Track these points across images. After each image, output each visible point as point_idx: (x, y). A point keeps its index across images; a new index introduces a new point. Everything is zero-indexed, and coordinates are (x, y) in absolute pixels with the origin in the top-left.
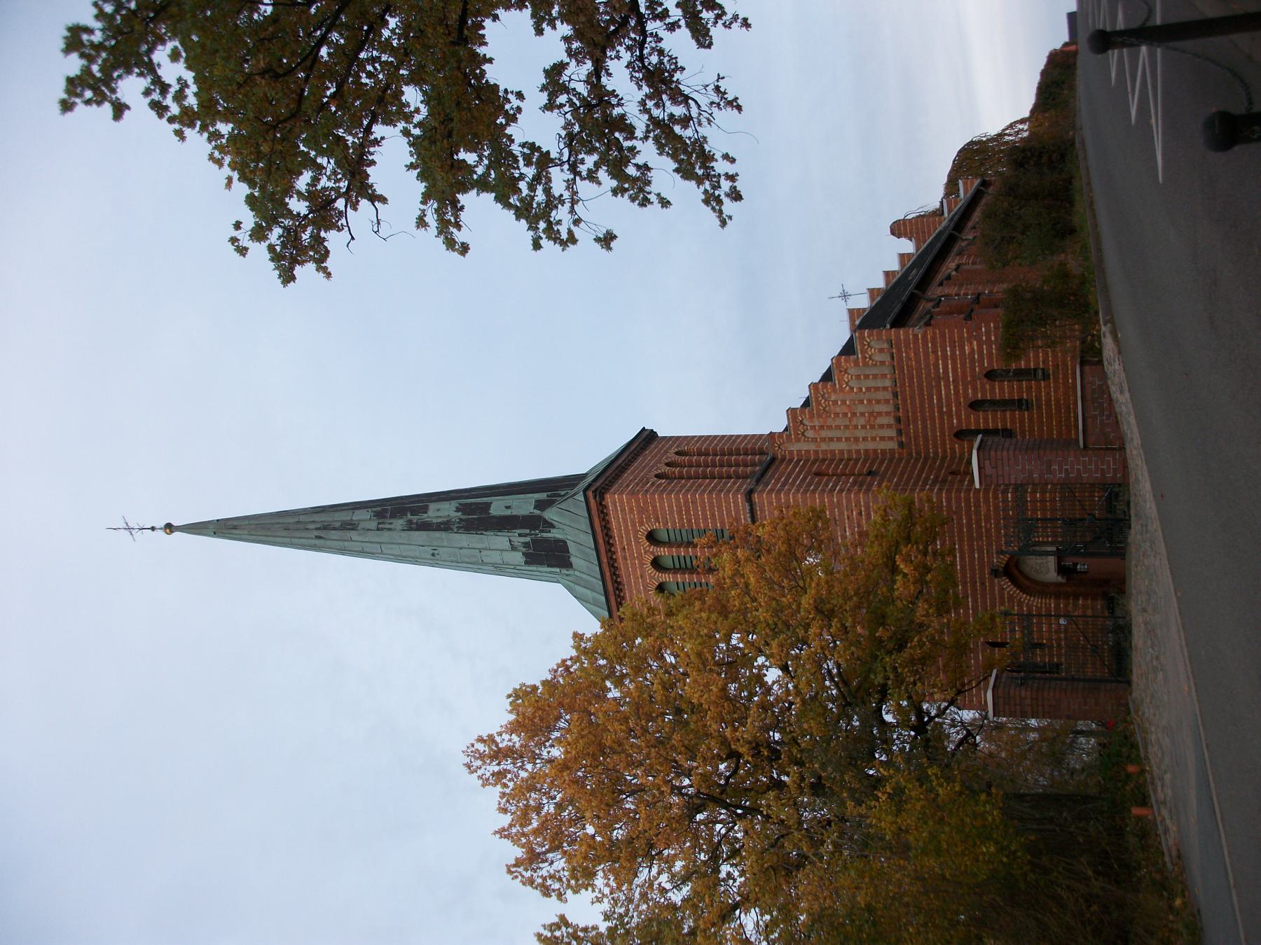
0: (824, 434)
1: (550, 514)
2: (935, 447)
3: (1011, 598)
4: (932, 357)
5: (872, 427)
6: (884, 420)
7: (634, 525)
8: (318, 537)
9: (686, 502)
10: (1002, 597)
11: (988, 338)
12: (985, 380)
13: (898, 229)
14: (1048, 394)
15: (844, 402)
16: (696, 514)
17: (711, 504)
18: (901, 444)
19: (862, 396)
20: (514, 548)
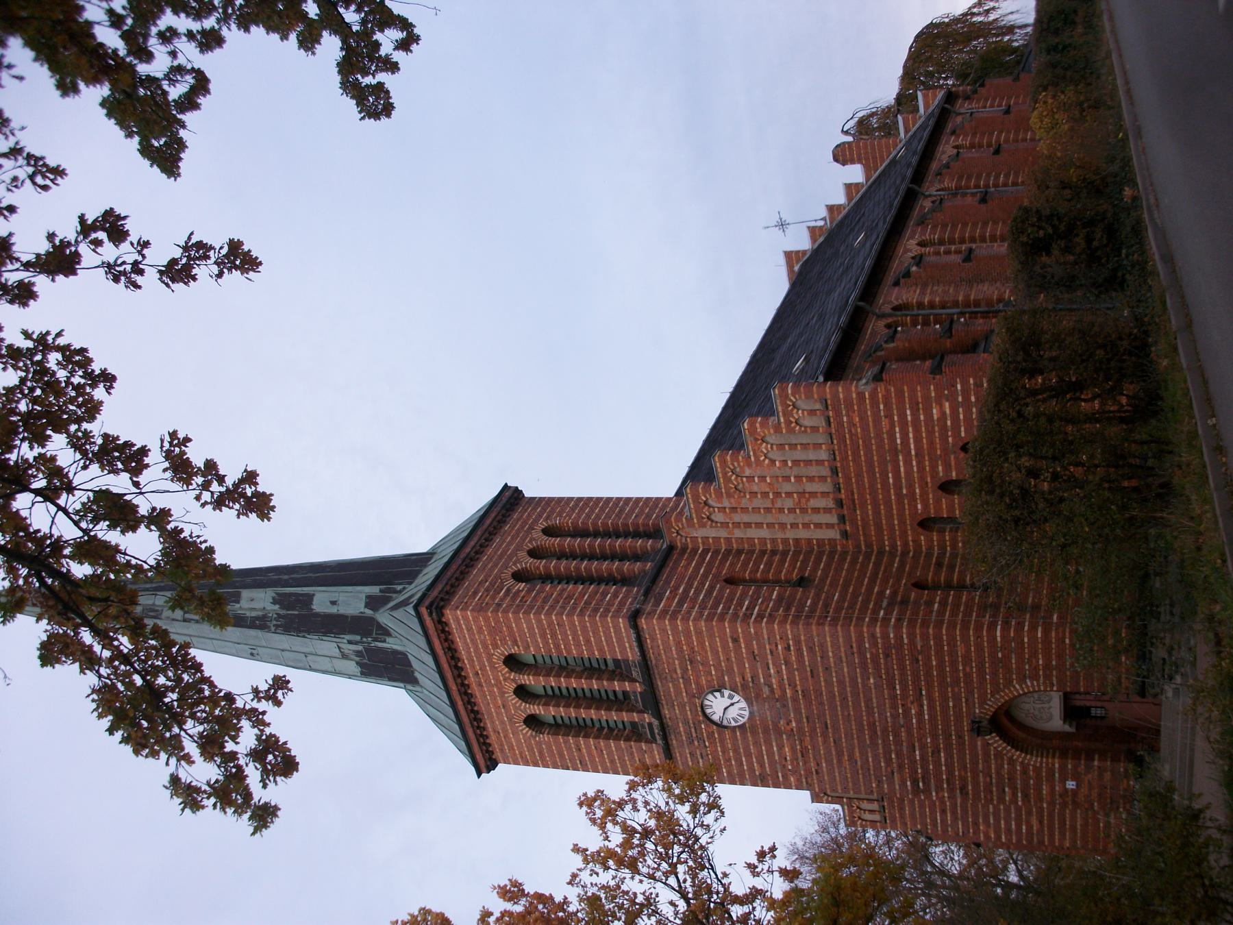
0: (737, 518)
3: (999, 755)
4: (885, 423)
6: (820, 503)
7: (485, 646)
9: (551, 624)
10: (986, 754)
15: (762, 478)
17: (584, 628)
18: (845, 534)
19: (788, 472)
20: (344, 656)
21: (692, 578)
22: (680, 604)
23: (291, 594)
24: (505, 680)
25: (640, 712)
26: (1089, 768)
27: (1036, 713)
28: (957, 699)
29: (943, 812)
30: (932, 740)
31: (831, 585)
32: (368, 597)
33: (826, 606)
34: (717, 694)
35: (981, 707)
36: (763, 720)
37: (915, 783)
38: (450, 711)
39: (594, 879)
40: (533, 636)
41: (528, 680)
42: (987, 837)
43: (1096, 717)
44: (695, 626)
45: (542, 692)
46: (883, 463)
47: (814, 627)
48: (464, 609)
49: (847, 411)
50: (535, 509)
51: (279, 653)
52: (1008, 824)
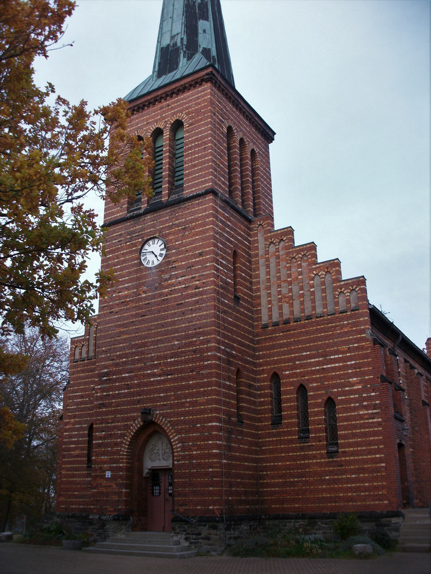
0: (273, 260)
2: (264, 356)
3: (127, 427)
5: (280, 300)
7: (186, 108)
9: (205, 143)
10: (127, 419)
11: (365, 399)
12: (325, 398)
14: (314, 457)
15: (300, 273)
16: (195, 153)
17: (204, 163)
18: (265, 326)
19: (306, 289)
20: (172, 37)
21: (235, 231)
22: (221, 221)
24: (166, 122)
25: (148, 201)
26: (120, 486)
27: (155, 451)
28: (165, 398)
29: (82, 397)
30: (136, 384)
31: (236, 316)
32: (209, 50)
33: (225, 312)
34: (163, 246)
35: (161, 414)
36: (145, 276)
37: (106, 374)
38: (145, 91)
39: (61, 113)
40: (196, 134)
41: (167, 134)
42: (67, 424)
43: (153, 490)
44: (210, 229)
45: (158, 145)
47: (213, 303)
48: (211, 94)
49: (351, 324)
51: (172, 3)
52: (75, 436)
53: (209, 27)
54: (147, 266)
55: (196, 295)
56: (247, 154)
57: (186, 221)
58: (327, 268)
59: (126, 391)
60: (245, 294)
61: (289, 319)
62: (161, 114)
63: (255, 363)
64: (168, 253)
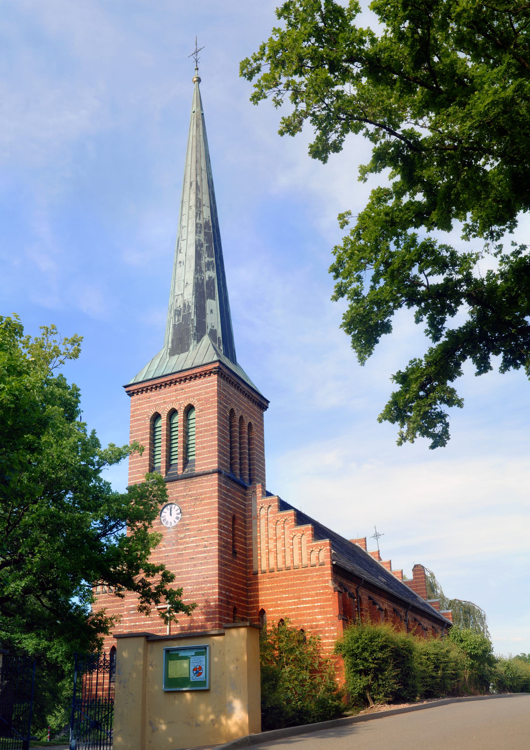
1: (206, 340)
7: (198, 395)
8: (191, 184)
13: (418, 569)
16: (204, 436)
23: (214, 287)
31: (234, 567)
34: (179, 511)
46: (294, 591)
50: (259, 417)
51: (183, 278)
53: (215, 308)
54: (166, 526)
55: (205, 552)
56: (244, 428)
57: (197, 493)
58: (303, 531)
59: (150, 622)
60: (241, 548)
61: (273, 569)
62: (176, 396)
63: (248, 601)
64: (182, 517)
